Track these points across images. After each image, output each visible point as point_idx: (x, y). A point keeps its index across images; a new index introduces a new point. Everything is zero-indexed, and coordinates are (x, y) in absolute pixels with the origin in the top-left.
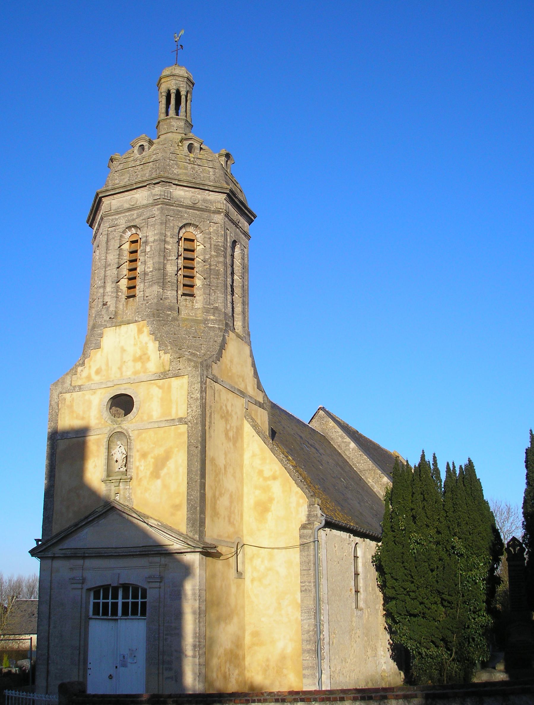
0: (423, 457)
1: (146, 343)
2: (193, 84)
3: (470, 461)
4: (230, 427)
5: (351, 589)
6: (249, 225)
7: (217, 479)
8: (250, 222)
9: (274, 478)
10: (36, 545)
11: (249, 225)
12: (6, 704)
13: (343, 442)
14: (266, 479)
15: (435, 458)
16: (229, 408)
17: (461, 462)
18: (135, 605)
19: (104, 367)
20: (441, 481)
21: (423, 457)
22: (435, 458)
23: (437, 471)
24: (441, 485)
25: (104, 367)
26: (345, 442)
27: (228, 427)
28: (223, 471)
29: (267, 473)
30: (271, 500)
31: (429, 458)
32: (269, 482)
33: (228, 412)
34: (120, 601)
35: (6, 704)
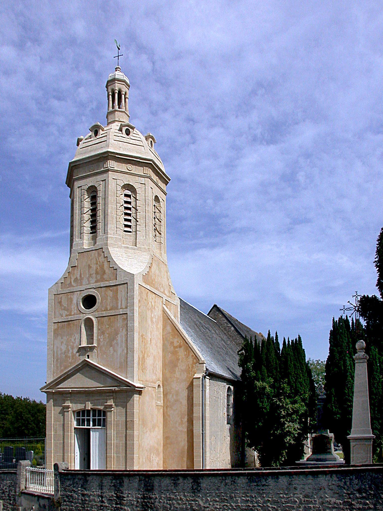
0: (269, 334)
1: (103, 262)
2: (129, 87)
3: (300, 338)
4: (154, 315)
5: (224, 413)
6: (166, 185)
7: (146, 347)
8: (166, 183)
9: (180, 347)
10: (135, 395)
11: (166, 185)
12: (381, 467)
13: (227, 326)
14: (175, 347)
15: (277, 336)
16: (153, 304)
17: (293, 337)
18: (99, 420)
19: (79, 278)
20: (279, 350)
21: (269, 334)
22: (277, 336)
23: (278, 344)
24: (280, 352)
25: (79, 278)
26: (229, 326)
27: (153, 316)
28: (150, 342)
29: (176, 344)
30: (178, 359)
31: (273, 335)
32: (177, 349)
33: (152, 306)
34: (91, 418)
35: (381, 467)
